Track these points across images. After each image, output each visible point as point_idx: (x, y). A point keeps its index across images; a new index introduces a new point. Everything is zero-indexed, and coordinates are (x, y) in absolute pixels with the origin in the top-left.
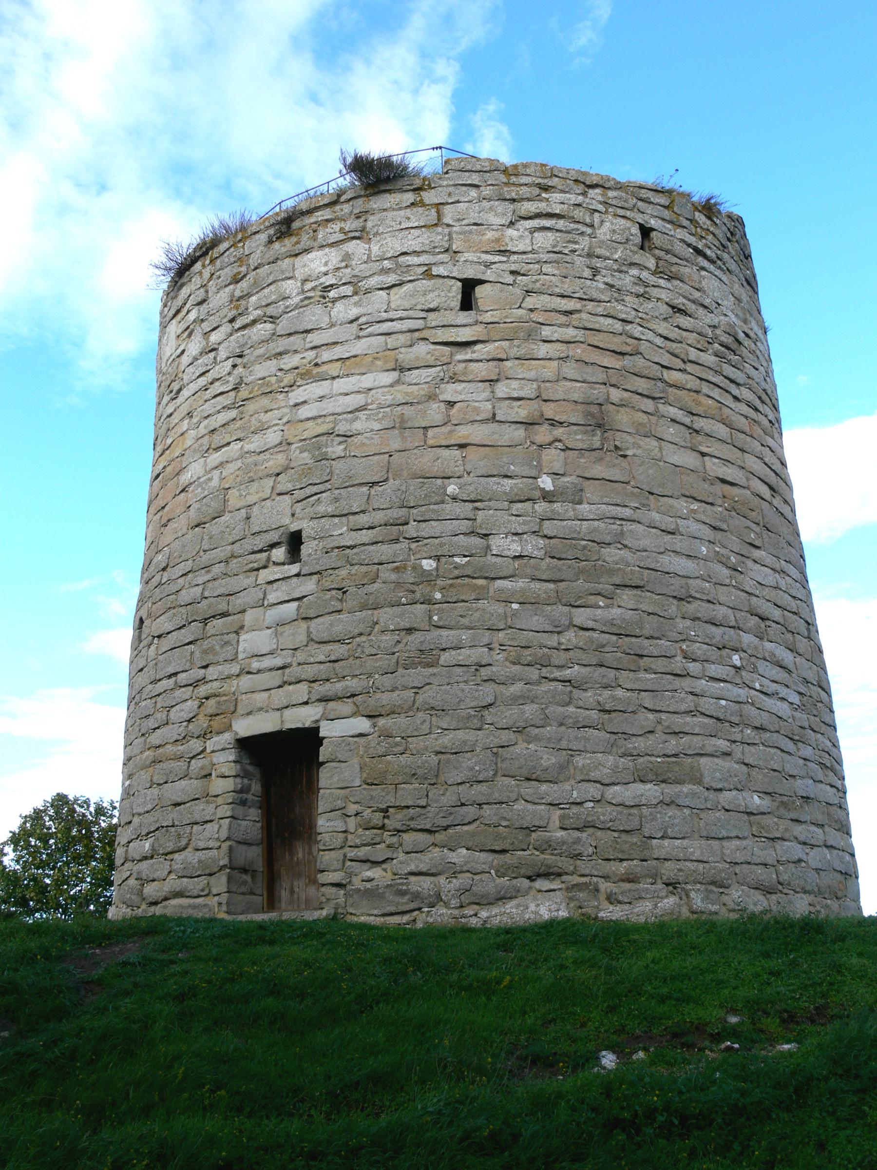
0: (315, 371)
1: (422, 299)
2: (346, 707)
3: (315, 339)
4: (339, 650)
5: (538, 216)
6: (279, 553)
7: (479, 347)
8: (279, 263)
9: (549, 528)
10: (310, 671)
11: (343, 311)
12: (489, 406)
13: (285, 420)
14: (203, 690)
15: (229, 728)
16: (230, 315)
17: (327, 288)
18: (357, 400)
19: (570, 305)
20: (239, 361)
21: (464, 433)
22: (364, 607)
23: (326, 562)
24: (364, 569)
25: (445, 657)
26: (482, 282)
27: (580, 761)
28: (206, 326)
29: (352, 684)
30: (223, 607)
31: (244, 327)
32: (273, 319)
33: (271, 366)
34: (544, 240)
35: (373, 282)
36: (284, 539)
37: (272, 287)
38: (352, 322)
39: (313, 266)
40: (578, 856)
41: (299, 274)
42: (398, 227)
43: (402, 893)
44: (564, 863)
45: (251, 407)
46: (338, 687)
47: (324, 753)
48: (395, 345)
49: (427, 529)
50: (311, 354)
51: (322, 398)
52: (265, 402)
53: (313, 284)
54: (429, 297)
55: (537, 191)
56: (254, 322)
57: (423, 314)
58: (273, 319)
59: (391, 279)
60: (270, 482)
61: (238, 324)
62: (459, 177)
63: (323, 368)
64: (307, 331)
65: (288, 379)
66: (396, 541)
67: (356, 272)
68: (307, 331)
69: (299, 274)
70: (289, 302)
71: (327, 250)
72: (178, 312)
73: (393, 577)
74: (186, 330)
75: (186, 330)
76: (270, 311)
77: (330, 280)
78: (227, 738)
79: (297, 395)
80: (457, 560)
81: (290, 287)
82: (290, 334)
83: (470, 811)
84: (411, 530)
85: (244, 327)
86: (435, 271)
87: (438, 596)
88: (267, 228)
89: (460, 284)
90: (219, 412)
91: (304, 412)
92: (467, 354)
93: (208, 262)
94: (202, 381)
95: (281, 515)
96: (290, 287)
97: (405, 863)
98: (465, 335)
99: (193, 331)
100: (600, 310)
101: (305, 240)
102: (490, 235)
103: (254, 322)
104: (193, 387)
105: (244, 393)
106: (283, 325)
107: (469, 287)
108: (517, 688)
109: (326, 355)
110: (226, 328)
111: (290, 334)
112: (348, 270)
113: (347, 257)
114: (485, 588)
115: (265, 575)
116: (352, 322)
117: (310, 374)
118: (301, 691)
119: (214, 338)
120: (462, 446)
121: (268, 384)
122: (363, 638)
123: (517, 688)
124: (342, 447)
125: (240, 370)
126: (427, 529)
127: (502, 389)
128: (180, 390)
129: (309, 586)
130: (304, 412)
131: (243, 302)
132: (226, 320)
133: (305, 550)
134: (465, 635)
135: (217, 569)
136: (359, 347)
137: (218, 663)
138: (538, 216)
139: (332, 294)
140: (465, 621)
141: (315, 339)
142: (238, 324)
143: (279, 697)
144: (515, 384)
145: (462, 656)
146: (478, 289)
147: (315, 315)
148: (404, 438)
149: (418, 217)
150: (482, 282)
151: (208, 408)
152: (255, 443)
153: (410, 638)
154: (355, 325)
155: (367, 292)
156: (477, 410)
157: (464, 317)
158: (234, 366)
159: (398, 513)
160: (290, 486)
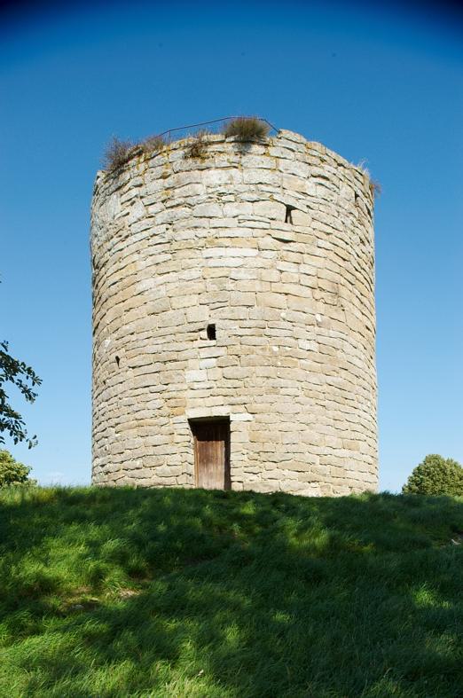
0: (216, 241)
1: (269, 212)
2: (242, 408)
3: (215, 222)
4: (237, 383)
5: (319, 176)
6: (204, 334)
7: (292, 244)
8: (192, 172)
9: (320, 339)
10: (225, 391)
11: (231, 209)
12: (297, 276)
13: (201, 265)
14: (166, 395)
15: (184, 413)
16: (163, 198)
17: (221, 194)
18: (239, 262)
19: (329, 230)
20: (169, 226)
21: (287, 288)
22: (248, 365)
23: (229, 341)
24: (247, 347)
25: (282, 391)
26: (295, 208)
27: (327, 438)
28: (146, 201)
29: (244, 399)
30: (175, 356)
31: (172, 207)
32: (190, 206)
33: (192, 233)
34: (321, 191)
35: (246, 196)
36: (206, 327)
37: (189, 186)
38: (234, 217)
39: (212, 179)
40: (325, 475)
41: (205, 182)
42: (257, 166)
43: (265, 486)
44: (322, 478)
45: (180, 254)
46: (238, 400)
47: (232, 427)
48: (258, 235)
49: (273, 332)
50: (213, 231)
51: (221, 257)
52: (189, 253)
53: (213, 190)
54: (273, 211)
55: (319, 162)
56: (178, 205)
57: (269, 221)
58: (190, 206)
59: (255, 197)
60: (196, 297)
61: (168, 204)
62: (287, 144)
63: (220, 240)
64: (211, 218)
65: (202, 242)
66: (261, 336)
67: (236, 188)
68: (211, 218)
69: (205, 182)
70: (200, 198)
71: (220, 171)
72: (119, 188)
73: (261, 352)
74: (128, 201)
75: (128, 201)
76: (189, 200)
77: (222, 190)
78: (184, 418)
79: (206, 253)
80: (287, 348)
81: (200, 189)
82: (201, 217)
83: (290, 455)
84: (268, 331)
85: (172, 207)
86: (276, 197)
87: (279, 364)
88: (185, 147)
89: (285, 208)
90: (160, 254)
91: (212, 263)
92: (286, 247)
93: (142, 160)
94: (146, 234)
95: (206, 317)
96: (200, 189)
97: (267, 475)
98: (287, 236)
99: (134, 202)
100: (339, 235)
101: (207, 163)
102: (299, 182)
103: (178, 205)
104: (139, 236)
105: (175, 245)
106: (198, 211)
107: (289, 209)
108: (308, 407)
109: (222, 233)
110: (159, 206)
111: (201, 217)
112: (232, 186)
113: (231, 178)
114: (297, 362)
115: (196, 344)
116: (234, 217)
117: (213, 242)
118: (220, 400)
119: (152, 209)
120: (286, 294)
121: (190, 243)
122: (248, 379)
123: (308, 407)
124: (233, 285)
125: (170, 231)
126: (273, 332)
127: (303, 268)
128: (127, 237)
129: (222, 351)
130: (212, 263)
131: (170, 192)
132: (160, 200)
133: (218, 334)
134: (290, 382)
135: (169, 338)
136: (238, 232)
137: (173, 383)
138: (319, 176)
139: (224, 198)
140: (290, 376)
141: (215, 222)
142: (168, 204)
143: (210, 401)
144: (307, 267)
145: (288, 391)
146: (293, 212)
147: (214, 209)
148: (262, 286)
149: (268, 162)
150: (295, 208)
151: (152, 250)
152: (186, 275)
153: (268, 381)
154: (236, 219)
155: (242, 201)
156: (292, 277)
157: (287, 226)
158: (167, 229)
159: (262, 323)
160: (207, 301)
